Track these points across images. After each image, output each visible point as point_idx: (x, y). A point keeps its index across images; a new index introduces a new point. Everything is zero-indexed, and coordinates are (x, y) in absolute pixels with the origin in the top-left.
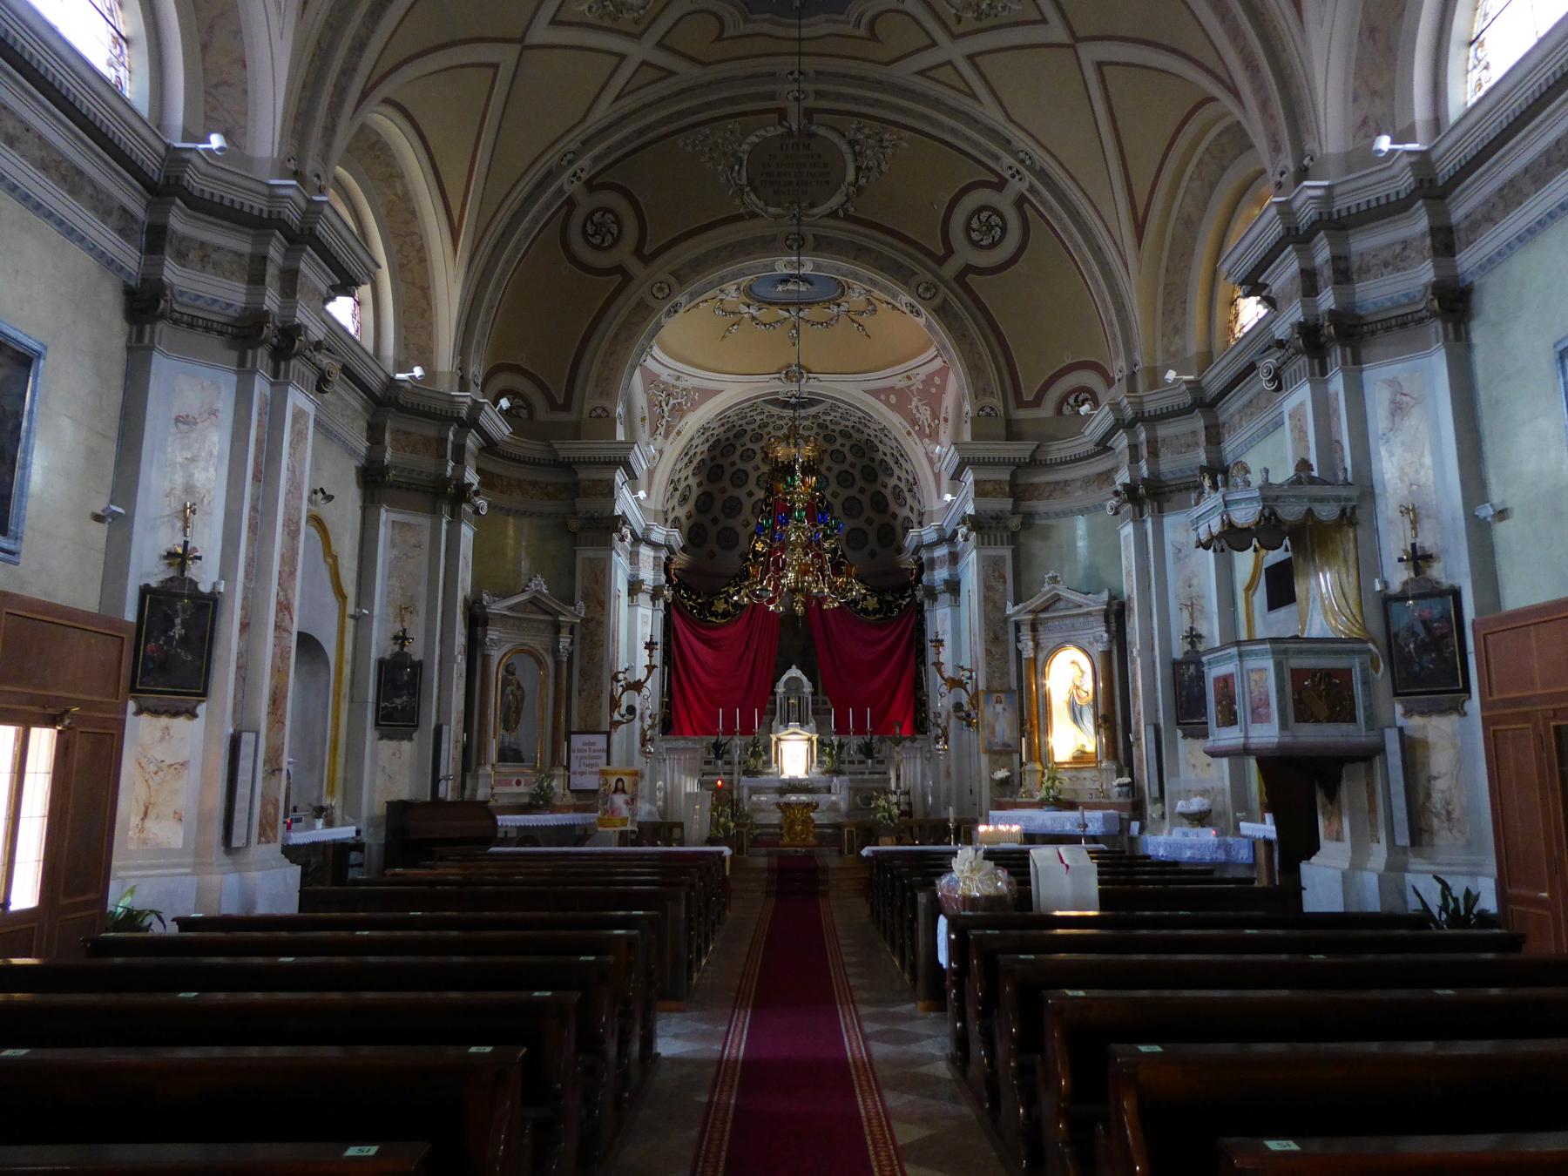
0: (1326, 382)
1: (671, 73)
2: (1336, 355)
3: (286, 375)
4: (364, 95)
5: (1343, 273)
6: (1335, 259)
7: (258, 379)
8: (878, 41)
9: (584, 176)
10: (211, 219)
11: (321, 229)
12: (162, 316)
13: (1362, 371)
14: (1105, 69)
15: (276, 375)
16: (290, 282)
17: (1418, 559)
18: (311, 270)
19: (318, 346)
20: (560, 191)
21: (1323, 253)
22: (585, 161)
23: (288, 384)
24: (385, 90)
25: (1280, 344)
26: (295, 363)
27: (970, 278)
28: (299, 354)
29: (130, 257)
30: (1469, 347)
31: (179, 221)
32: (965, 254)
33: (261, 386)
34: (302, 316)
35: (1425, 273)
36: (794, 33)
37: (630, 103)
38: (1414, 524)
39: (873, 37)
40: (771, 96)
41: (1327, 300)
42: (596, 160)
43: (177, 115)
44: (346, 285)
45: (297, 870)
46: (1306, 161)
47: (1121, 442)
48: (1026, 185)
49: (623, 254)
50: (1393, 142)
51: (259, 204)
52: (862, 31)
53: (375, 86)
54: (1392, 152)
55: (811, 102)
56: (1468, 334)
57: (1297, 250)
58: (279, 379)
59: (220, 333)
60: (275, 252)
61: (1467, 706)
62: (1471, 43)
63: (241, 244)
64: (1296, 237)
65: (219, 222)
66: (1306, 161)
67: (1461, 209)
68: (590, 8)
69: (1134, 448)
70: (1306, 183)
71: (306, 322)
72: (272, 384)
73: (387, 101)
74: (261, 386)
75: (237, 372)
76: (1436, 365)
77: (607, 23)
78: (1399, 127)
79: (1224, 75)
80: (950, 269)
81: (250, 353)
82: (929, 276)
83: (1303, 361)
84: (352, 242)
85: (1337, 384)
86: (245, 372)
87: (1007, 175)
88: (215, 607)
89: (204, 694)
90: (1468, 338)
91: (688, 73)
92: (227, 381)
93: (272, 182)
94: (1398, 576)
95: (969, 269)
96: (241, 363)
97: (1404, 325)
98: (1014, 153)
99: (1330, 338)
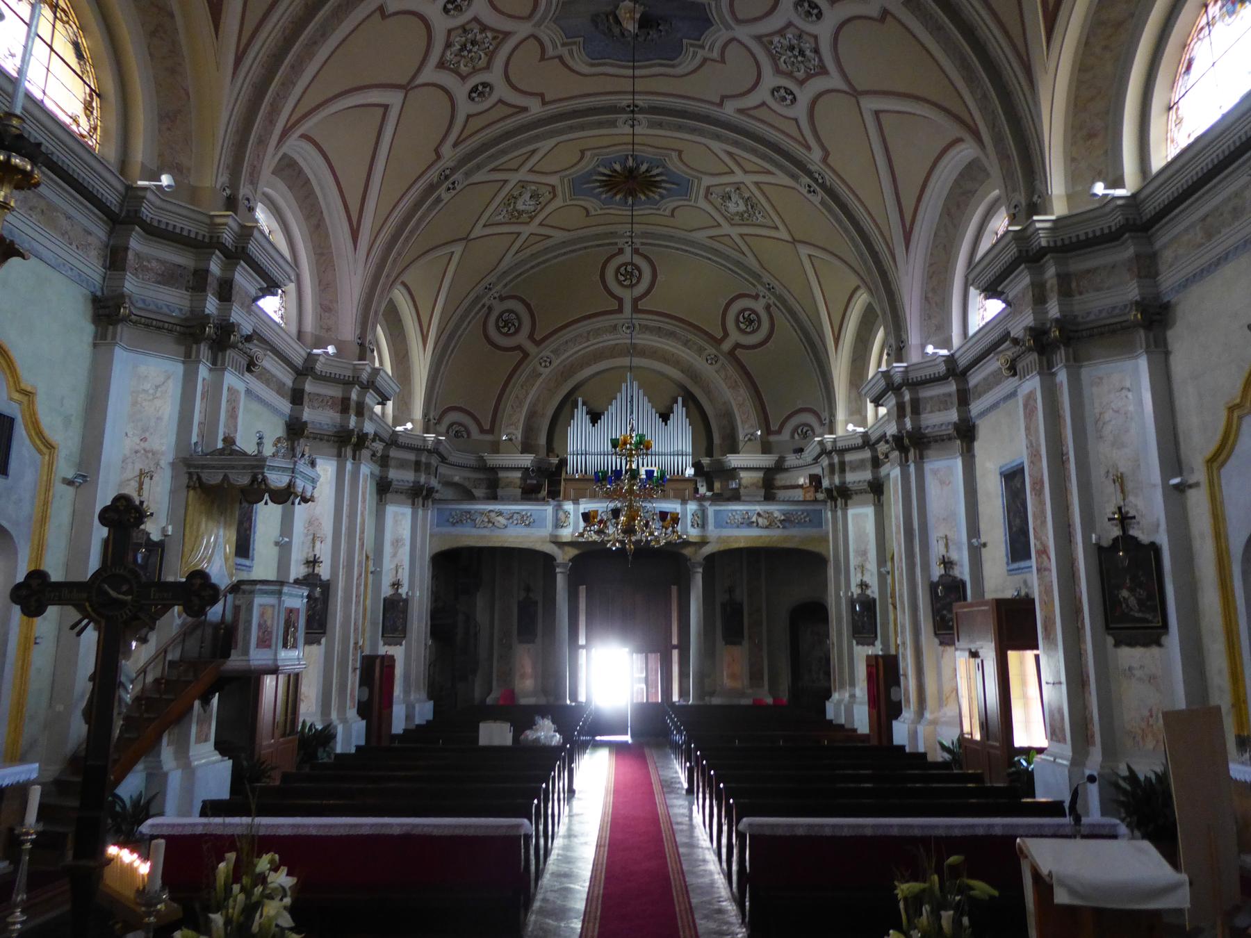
0: (1054, 374)
2: (1060, 355)
3: (223, 363)
4: (285, 134)
5: (916, 409)
6: (912, 400)
7: (201, 367)
11: (252, 248)
12: (125, 319)
13: (1081, 367)
14: (881, 115)
15: (214, 363)
16: (226, 292)
17: (947, 563)
18: (244, 279)
19: (248, 339)
21: (836, 460)
22: (499, 287)
24: (302, 129)
25: (1016, 342)
26: (230, 353)
28: (234, 346)
29: (285, 406)
30: (973, 456)
31: (309, 386)
32: (735, 336)
33: (203, 372)
34: (237, 315)
35: (953, 415)
36: (627, 85)
37: (521, 256)
38: (947, 546)
39: (672, 215)
41: (1053, 310)
43: (140, 152)
44: (271, 287)
45: (229, 763)
46: (1035, 198)
47: (825, 461)
49: (522, 338)
50: (1106, 188)
53: (245, 51)
56: (1165, 340)
57: (1029, 268)
58: (217, 366)
59: (170, 331)
60: (215, 267)
61: (1164, 640)
62: (1170, 108)
63: (411, 457)
66: (1035, 198)
67: (975, 379)
69: (831, 466)
70: (1035, 218)
71: (240, 321)
72: (211, 370)
73: (305, 137)
74: (420, 512)
75: (184, 362)
76: (1141, 367)
77: (514, 220)
80: (726, 346)
82: (714, 351)
83: (1034, 356)
84: (287, 268)
85: (1062, 376)
86: (190, 360)
88: (163, 551)
89: (324, 633)
90: (1165, 344)
92: (178, 369)
94: (856, 591)
95: (738, 345)
96: (188, 355)
97: (1114, 332)
98: (763, 284)
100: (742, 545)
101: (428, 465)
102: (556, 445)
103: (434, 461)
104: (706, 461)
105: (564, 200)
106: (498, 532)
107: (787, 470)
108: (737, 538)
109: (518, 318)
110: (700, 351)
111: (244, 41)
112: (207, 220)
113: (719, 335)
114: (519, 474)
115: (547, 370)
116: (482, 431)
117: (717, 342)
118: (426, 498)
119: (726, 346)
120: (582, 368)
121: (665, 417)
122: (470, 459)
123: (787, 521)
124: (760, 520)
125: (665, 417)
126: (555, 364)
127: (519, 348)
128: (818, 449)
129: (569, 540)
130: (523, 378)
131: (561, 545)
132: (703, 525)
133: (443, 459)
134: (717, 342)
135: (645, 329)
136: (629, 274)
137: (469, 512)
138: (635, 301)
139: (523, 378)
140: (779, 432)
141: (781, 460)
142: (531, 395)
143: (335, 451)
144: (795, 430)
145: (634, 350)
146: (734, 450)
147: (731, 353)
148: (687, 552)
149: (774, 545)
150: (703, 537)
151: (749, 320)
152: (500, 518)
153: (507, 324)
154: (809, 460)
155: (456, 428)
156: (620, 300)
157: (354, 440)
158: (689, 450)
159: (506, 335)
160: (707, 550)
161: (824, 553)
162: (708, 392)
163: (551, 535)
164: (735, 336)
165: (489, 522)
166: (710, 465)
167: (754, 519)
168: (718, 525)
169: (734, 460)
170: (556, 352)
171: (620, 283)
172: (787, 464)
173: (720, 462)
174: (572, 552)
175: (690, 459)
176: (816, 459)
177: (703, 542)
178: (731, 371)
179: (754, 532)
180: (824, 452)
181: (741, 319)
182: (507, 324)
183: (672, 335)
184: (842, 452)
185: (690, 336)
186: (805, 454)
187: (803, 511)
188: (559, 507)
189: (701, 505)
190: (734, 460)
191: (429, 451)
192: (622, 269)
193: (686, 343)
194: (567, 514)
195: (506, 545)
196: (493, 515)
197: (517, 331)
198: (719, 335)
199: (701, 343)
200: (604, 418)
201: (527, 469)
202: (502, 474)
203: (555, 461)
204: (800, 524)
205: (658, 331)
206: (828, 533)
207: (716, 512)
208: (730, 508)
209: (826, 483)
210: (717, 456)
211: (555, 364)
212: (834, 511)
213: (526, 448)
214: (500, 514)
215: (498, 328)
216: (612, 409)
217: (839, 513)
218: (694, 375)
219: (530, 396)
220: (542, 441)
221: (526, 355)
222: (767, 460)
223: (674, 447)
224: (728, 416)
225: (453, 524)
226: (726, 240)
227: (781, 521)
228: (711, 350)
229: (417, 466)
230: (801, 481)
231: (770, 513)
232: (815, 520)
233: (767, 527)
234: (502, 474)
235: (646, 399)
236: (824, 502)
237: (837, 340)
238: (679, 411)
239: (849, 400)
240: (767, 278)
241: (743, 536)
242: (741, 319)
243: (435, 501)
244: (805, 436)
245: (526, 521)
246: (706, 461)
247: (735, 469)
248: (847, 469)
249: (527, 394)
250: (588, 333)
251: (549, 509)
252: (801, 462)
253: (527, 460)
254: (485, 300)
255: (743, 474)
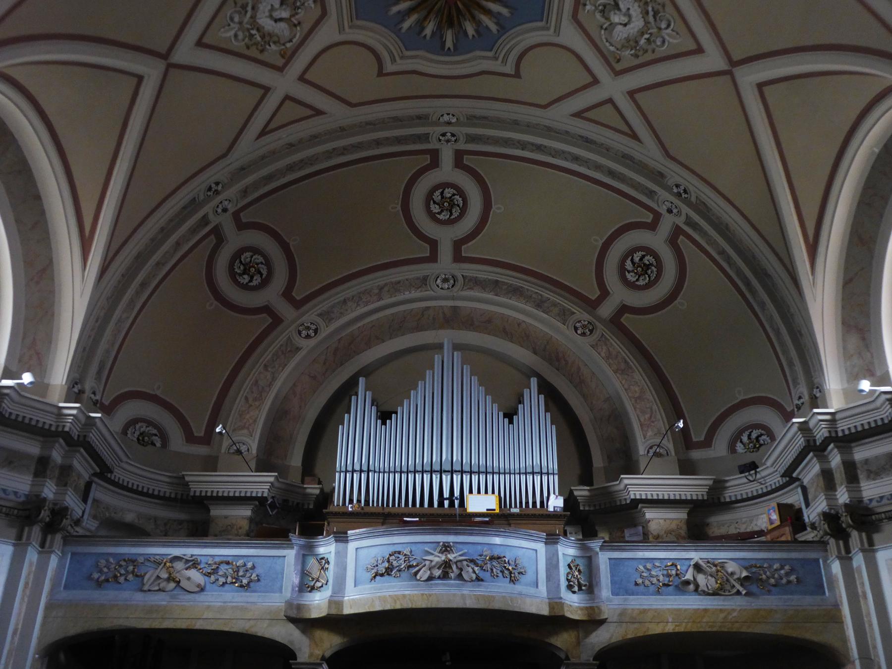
0: (851, 559)
1: (319, 112)
5: (852, 472)
8: (511, 422)
9: (232, 208)
10: (9, 430)
15: (42, 545)
20: (205, 221)
21: (836, 460)
22: (232, 192)
23: (51, 552)
27: (627, 319)
32: (619, 295)
40: (425, 138)
41: (843, 496)
42: (245, 192)
47: (811, 471)
48: (683, 218)
49: (271, 295)
51: (49, 421)
52: (509, 69)
54: (872, 392)
55: (462, 146)
63: (33, 448)
64: (814, 448)
65: (21, 433)
68: (236, 36)
69: (827, 476)
70: (816, 410)
72: (40, 553)
74: (32, 555)
75: (14, 545)
77: (254, 52)
78: (878, 373)
79: (791, 269)
80: (606, 310)
81: (26, 529)
86: (20, 542)
87: (663, 210)
91: (338, 114)
93: (61, 405)
96: (19, 537)
99: (849, 526)
100: (670, 628)
101: (65, 471)
102: (319, 470)
103: (82, 466)
104: (581, 492)
105: (341, 29)
106: (186, 600)
107: (729, 506)
108: (658, 617)
109: (268, 263)
110: (564, 315)
111: (111, 255)
112: (55, 411)
113: (594, 294)
114: (246, 512)
115: (312, 342)
116: (190, 438)
117: (592, 305)
118: (51, 528)
119: (606, 310)
120: (369, 345)
121: (510, 416)
122: (158, 481)
123: (754, 581)
124: (701, 579)
125: (510, 416)
126: (322, 335)
127: (267, 309)
128: (800, 441)
129: (323, 614)
130: (268, 356)
131: (307, 625)
132: (589, 587)
133: (103, 471)
134: (592, 305)
135: (474, 283)
136: (449, 204)
137: (132, 561)
138: (458, 245)
139: (268, 356)
140: (707, 443)
141: (718, 487)
142: (281, 379)
143: (13, 532)
144: (736, 438)
145: (453, 319)
146: (631, 468)
147: (615, 322)
148: (562, 641)
149: (735, 628)
150: (591, 610)
151: (646, 267)
152: (194, 574)
153: (249, 269)
154: (776, 480)
155: (142, 427)
156: (433, 244)
157: (45, 514)
158: (554, 466)
159: (245, 287)
160: (601, 638)
161: (837, 644)
162: (579, 382)
163: (289, 604)
164: (619, 295)
165: (170, 579)
166: (590, 500)
167: (689, 576)
168: (619, 588)
169: (634, 486)
170: (327, 316)
171: (433, 216)
172: (730, 494)
173: (607, 494)
174: (330, 642)
175: (555, 480)
176: (790, 476)
177: (593, 622)
178: (616, 345)
179: (691, 602)
180: (814, 448)
181: (629, 265)
182: (249, 269)
183: (516, 292)
184: (847, 441)
185: (546, 294)
186: (763, 472)
187: (783, 562)
188: (308, 551)
189: (584, 548)
190: (634, 486)
191: (67, 437)
192: (437, 196)
193: (540, 304)
194: (323, 562)
195: (199, 625)
196: (179, 565)
197: (265, 283)
198: (594, 294)
199: (567, 305)
200: (403, 411)
201: (262, 500)
202: (216, 512)
203: (313, 489)
204: (780, 587)
205: (495, 286)
206: (837, 606)
207: (615, 564)
208: (640, 554)
209: (811, 515)
210: (599, 482)
211: (322, 335)
212: (846, 558)
213: (263, 465)
214: (194, 564)
215: (233, 275)
216: (416, 397)
217: (858, 560)
218: (554, 356)
219: (278, 384)
220: (296, 460)
221: (277, 321)
222: (690, 487)
223: (529, 461)
224: (617, 420)
225: (99, 584)
226: (606, 114)
227: (743, 581)
228: (582, 315)
229: (42, 467)
230: (762, 523)
231: (719, 566)
232: (811, 580)
233: (715, 594)
234: (216, 512)
235: (475, 379)
236: (821, 544)
237: (813, 249)
238: (534, 402)
239: (846, 355)
240: (676, 175)
241: (671, 611)
242: (629, 265)
243: (68, 540)
244: (756, 445)
245: (243, 579)
246: (581, 492)
247: (636, 502)
248: (862, 476)
249: (274, 379)
250: (381, 289)
251: (289, 556)
252: (754, 488)
253: (261, 484)
254: (207, 209)
255: (650, 514)
